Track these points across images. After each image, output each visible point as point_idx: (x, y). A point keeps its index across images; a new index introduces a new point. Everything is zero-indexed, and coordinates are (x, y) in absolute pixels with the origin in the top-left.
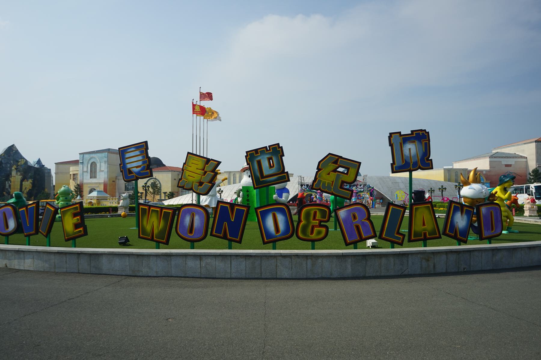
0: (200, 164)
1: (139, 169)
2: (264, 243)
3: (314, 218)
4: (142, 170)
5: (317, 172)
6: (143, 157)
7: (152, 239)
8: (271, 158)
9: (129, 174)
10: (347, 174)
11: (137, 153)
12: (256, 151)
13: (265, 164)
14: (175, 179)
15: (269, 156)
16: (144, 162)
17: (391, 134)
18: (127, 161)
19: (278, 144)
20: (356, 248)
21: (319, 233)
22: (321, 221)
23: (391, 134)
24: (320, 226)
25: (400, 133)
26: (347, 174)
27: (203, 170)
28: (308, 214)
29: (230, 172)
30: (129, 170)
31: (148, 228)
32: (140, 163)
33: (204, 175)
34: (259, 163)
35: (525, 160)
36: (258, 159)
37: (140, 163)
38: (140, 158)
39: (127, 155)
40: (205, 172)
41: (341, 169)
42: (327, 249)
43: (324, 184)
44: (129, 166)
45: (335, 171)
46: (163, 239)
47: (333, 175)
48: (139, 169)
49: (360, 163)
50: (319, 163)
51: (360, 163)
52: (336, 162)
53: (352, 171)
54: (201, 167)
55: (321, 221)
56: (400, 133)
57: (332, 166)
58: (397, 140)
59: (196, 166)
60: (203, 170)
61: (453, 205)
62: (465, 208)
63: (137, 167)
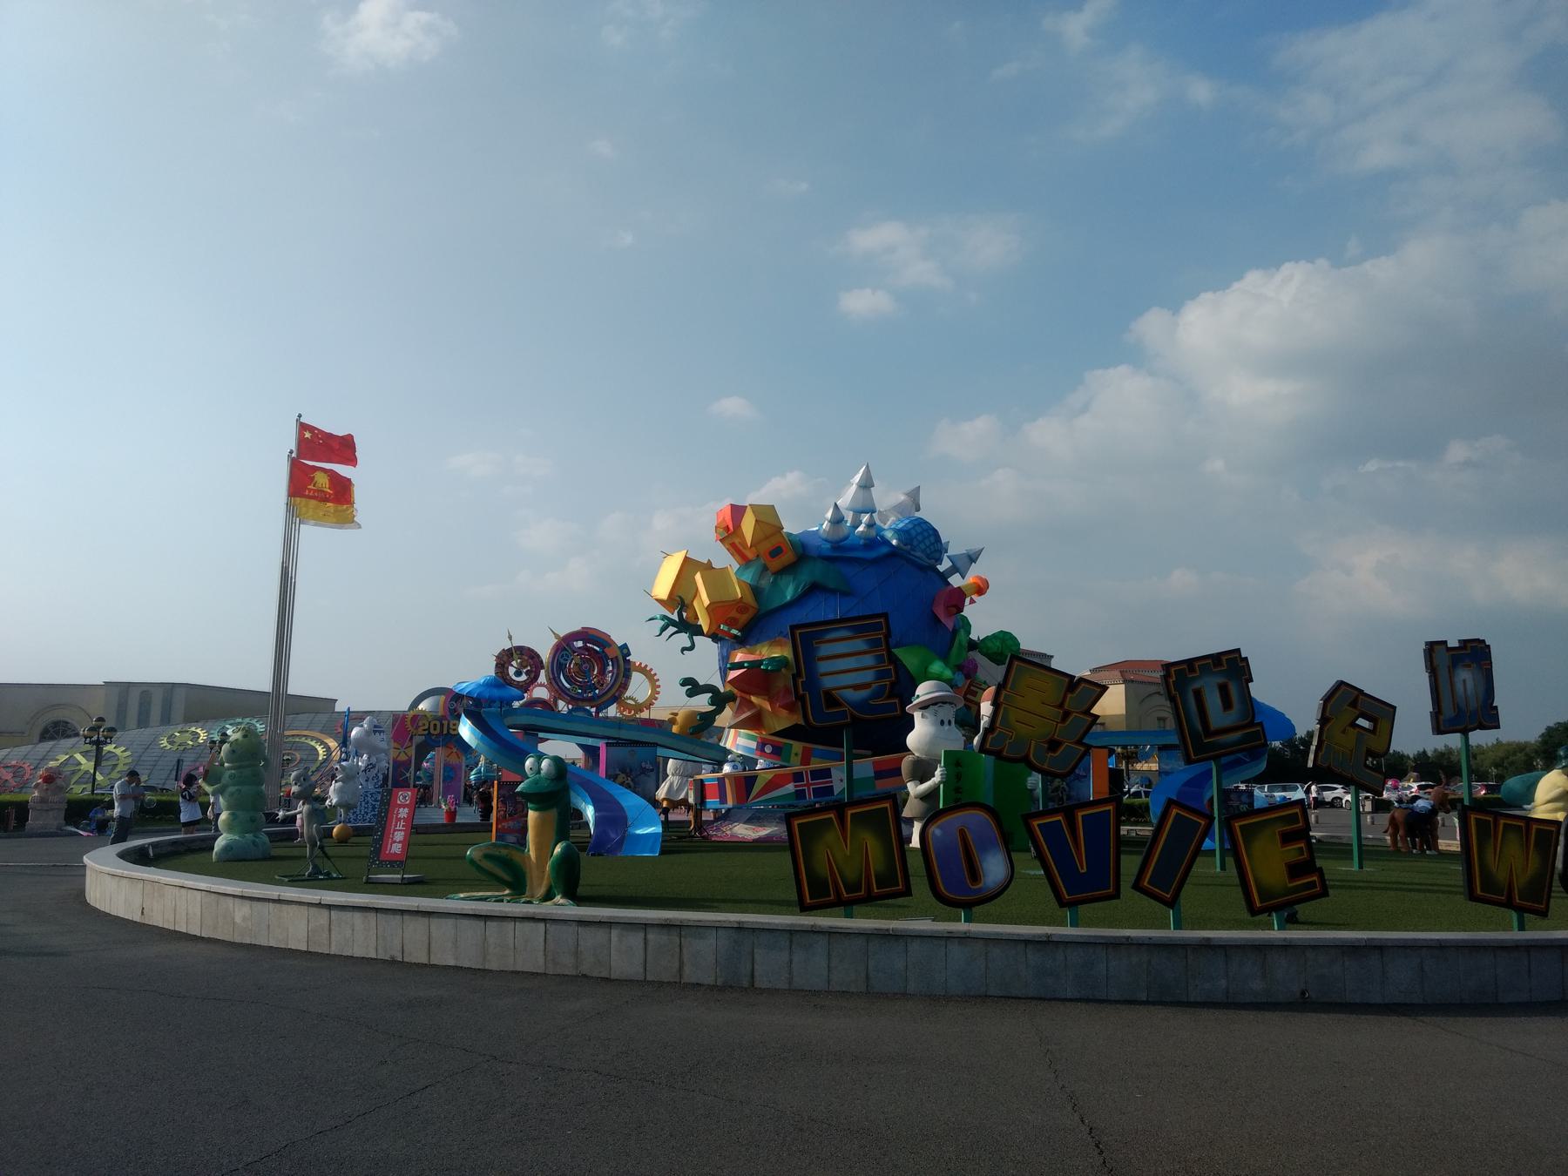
1: (864, 693)
2: (1253, 911)
4: (876, 696)
6: (880, 659)
7: (1509, 904)
9: (828, 707)
10: (1373, 731)
11: (859, 644)
15: (1221, 680)
16: (881, 675)
18: (824, 667)
19: (1238, 651)
20: (1292, 921)
25: (1445, 642)
27: (1061, 706)
30: (828, 693)
31: (1501, 876)
32: (868, 676)
33: (1064, 719)
34: (1198, 694)
36: (1197, 685)
37: (868, 676)
38: (868, 660)
39: (825, 649)
40: (1067, 714)
41: (1362, 722)
42: (1416, 929)
44: (828, 683)
46: (1285, 907)
47: (1352, 732)
48: (864, 693)
52: (1354, 704)
56: (1445, 642)
58: (1442, 660)
61: (1175, 811)
62: (1035, 823)
63: (856, 687)
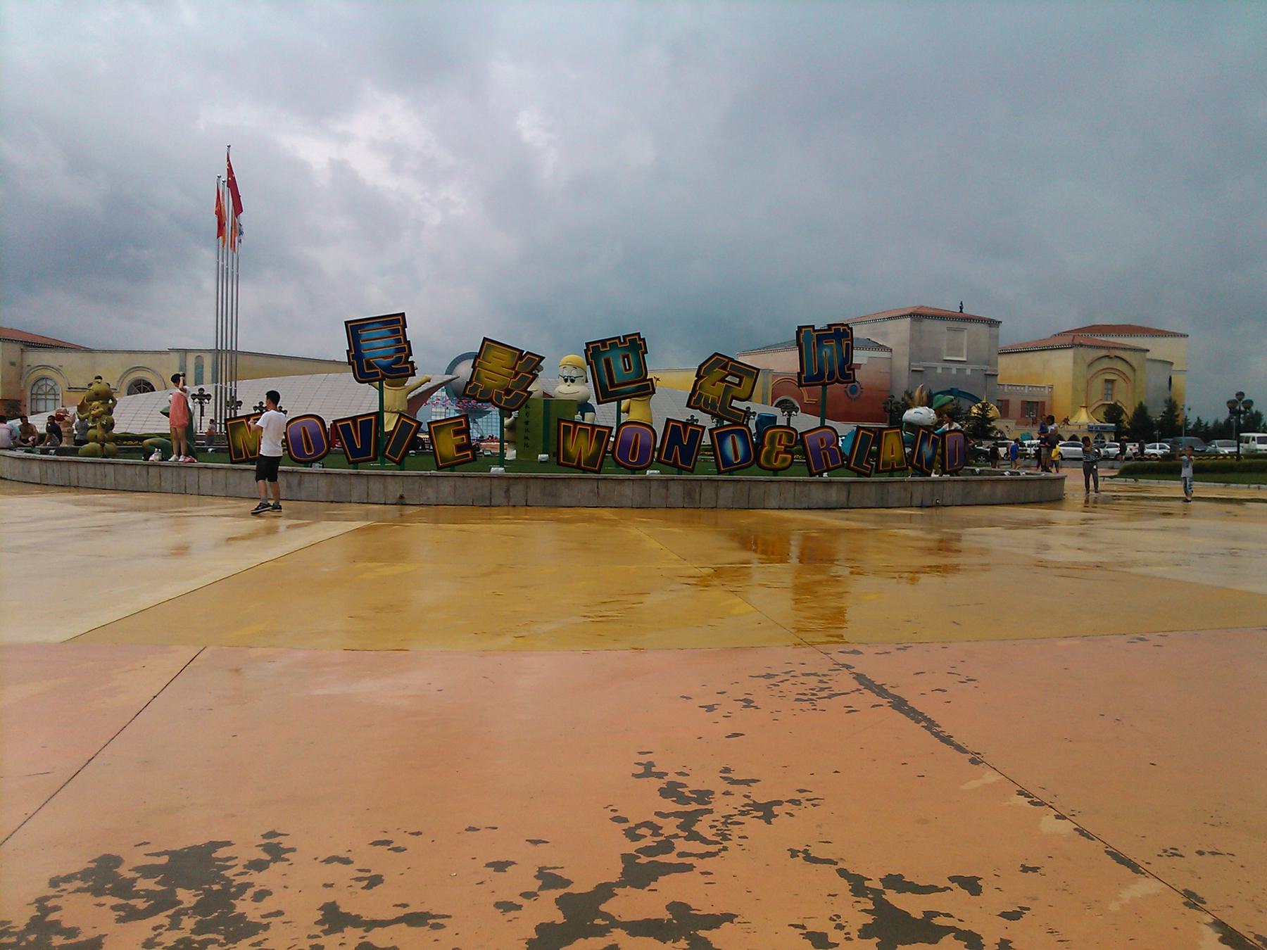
0: (507, 359)
3: (779, 443)
5: (696, 382)
8: (627, 356)
12: (603, 342)
13: (618, 364)
14: (13, 364)
17: (800, 328)
21: (784, 460)
22: (786, 447)
23: (800, 328)
24: (786, 452)
26: (739, 385)
28: (773, 438)
29: (186, 351)
34: (608, 362)
35: (886, 355)
36: (607, 356)
43: (707, 399)
45: (723, 380)
49: (403, 315)
50: (700, 367)
51: (403, 315)
53: (747, 381)
54: (510, 363)
55: (786, 447)
57: (719, 373)
59: (498, 365)
60: (513, 369)
